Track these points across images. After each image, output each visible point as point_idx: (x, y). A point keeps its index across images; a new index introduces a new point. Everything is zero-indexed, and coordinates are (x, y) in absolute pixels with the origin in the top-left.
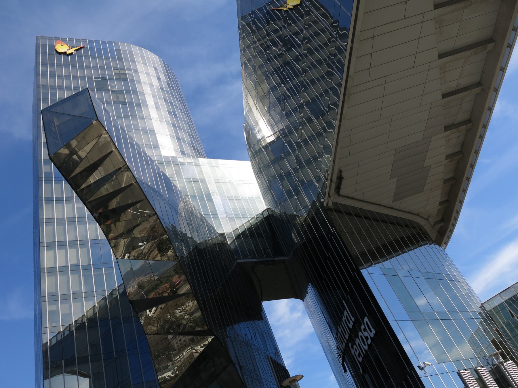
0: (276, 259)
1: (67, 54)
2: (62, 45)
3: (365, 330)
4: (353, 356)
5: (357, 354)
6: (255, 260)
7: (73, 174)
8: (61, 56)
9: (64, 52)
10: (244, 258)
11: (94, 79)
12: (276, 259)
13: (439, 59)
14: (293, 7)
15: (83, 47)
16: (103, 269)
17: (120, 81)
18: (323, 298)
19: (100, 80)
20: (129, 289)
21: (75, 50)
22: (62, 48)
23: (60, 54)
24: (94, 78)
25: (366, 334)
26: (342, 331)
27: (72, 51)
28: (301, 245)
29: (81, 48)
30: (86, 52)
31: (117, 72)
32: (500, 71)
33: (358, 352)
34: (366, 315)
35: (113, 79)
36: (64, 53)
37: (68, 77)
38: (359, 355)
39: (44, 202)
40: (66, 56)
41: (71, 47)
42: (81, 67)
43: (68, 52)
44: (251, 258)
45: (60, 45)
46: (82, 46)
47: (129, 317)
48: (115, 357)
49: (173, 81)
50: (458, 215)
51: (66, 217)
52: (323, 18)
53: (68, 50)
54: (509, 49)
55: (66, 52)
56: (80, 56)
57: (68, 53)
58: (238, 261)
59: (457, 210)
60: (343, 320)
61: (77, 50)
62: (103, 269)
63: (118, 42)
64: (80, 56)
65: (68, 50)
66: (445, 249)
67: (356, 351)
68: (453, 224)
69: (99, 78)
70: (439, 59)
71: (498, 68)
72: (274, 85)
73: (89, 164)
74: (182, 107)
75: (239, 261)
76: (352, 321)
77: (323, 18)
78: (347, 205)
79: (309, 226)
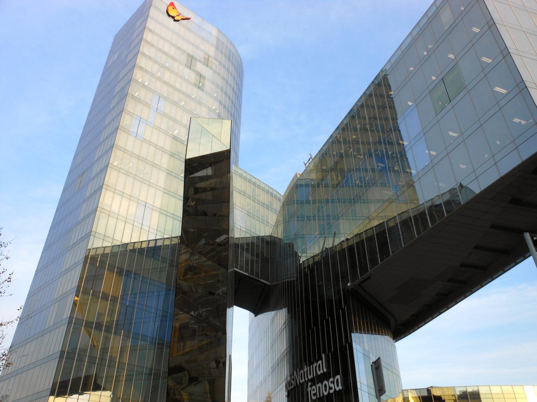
0: (262, 280)
2: (174, 9)
3: (333, 382)
4: (307, 392)
5: (313, 392)
6: (247, 274)
7: (192, 176)
11: (363, 184)
13: (490, 228)
16: (97, 266)
21: (182, 19)
23: (169, 16)
25: (332, 385)
26: (307, 371)
33: (315, 392)
34: (339, 374)
38: (314, 395)
48: (127, 305)
53: (177, 16)
57: (176, 19)
60: (314, 365)
62: (97, 266)
65: (177, 16)
66: (395, 342)
67: (314, 390)
70: (490, 228)
73: (203, 171)
75: (236, 269)
76: (322, 371)
78: (233, 195)
79: (306, 274)
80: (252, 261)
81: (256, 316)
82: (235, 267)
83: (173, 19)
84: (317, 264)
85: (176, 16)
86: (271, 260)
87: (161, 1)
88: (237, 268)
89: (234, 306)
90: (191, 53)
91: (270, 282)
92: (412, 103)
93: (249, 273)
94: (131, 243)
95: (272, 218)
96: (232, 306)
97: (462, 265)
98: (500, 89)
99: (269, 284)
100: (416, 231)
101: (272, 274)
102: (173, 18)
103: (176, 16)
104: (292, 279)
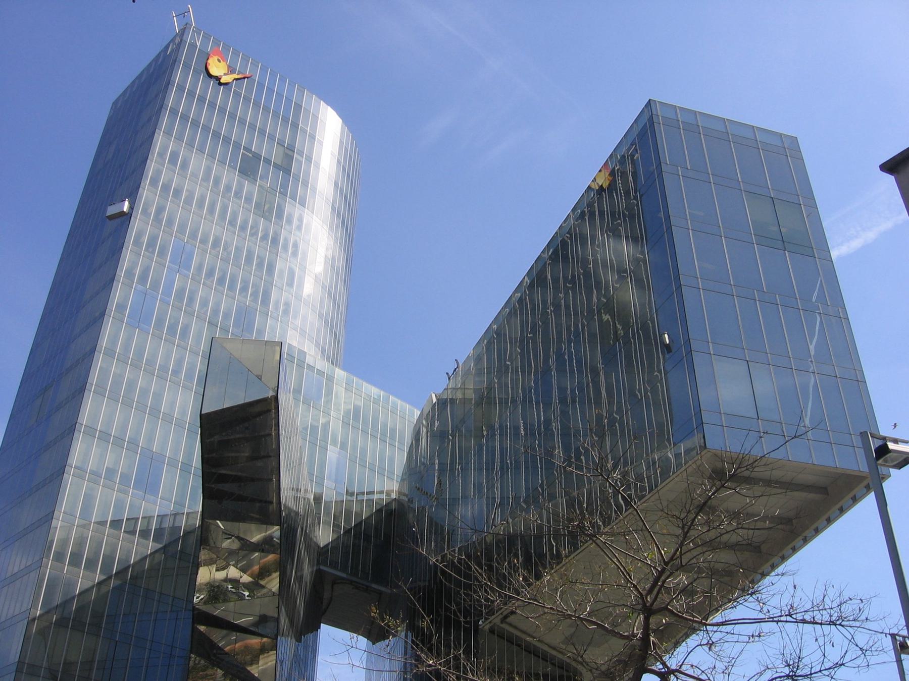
1: (220, 82)
2: (219, 61)
6: (344, 575)
9: (217, 76)
10: (331, 566)
12: (374, 586)
15: (247, 78)
17: (279, 171)
18: (510, 470)
19: (251, 155)
22: (217, 68)
23: (210, 76)
24: (243, 149)
29: (244, 78)
32: (837, 510)
36: (218, 79)
41: (231, 70)
44: (340, 571)
45: (216, 58)
49: (349, 236)
50: (839, 515)
52: (496, 492)
53: (225, 74)
54: (865, 490)
55: (220, 79)
57: (222, 81)
59: (843, 507)
61: (237, 79)
63: (201, 31)
65: (225, 74)
68: (855, 496)
71: (791, 546)
77: (496, 492)
81: (373, 644)
83: (218, 81)
102: (216, 80)
103: (223, 74)
104: (422, 584)
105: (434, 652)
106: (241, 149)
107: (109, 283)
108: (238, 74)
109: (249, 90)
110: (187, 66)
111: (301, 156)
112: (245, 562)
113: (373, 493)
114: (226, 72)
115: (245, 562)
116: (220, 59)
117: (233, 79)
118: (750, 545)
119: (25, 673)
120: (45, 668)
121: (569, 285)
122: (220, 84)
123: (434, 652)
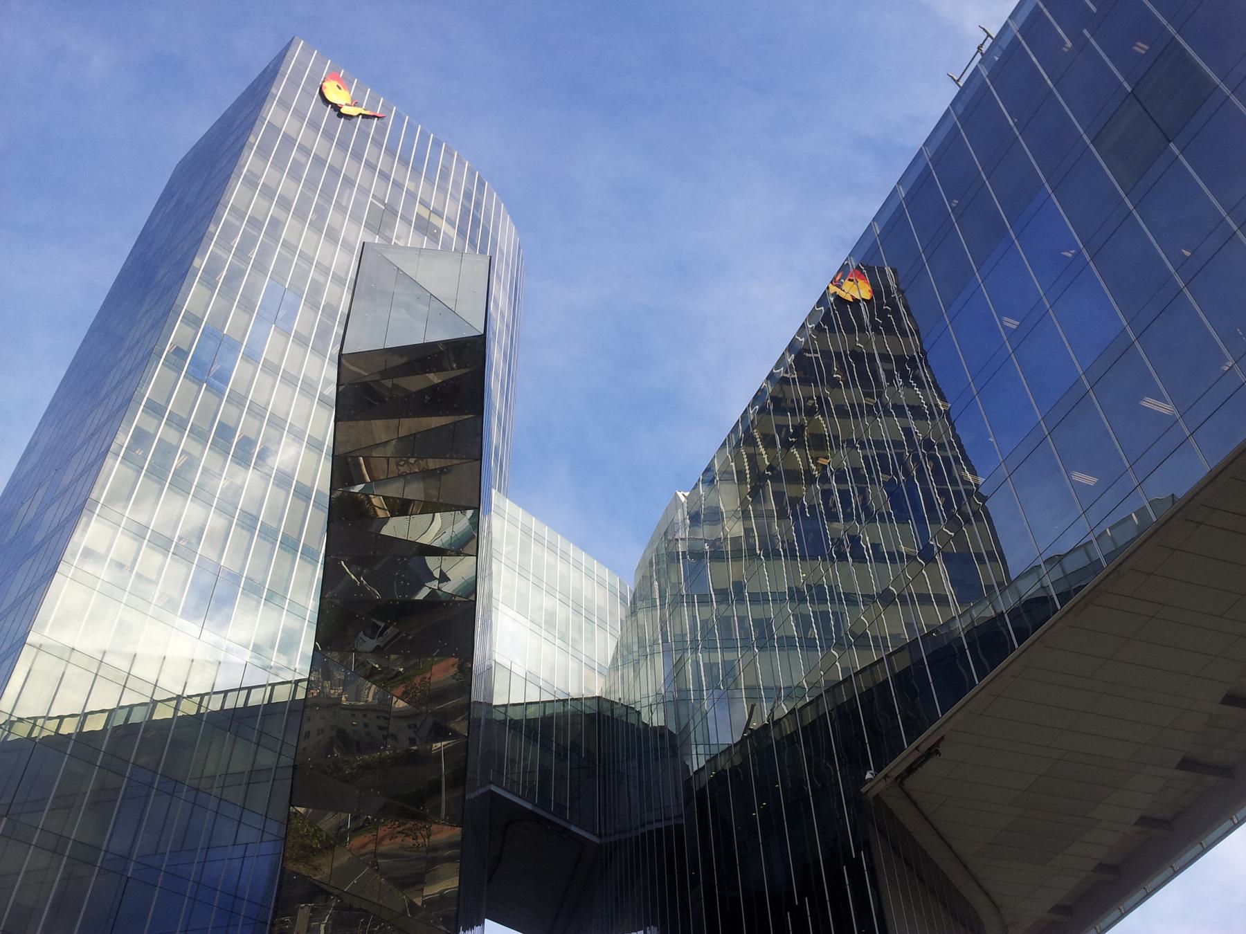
0: (574, 829)
1: (340, 112)
6: (529, 806)
8: (325, 107)
9: (336, 104)
14: (851, 300)
20: (266, 759)
21: (360, 114)
22: (336, 94)
27: (353, 111)
28: (645, 833)
29: (374, 116)
30: (381, 131)
31: (425, 213)
35: (374, 168)
36: (336, 108)
37: (319, 161)
39: (142, 407)
40: (336, 117)
42: (357, 156)
43: (344, 110)
46: (378, 113)
47: (221, 799)
48: (129, 875)
51: (245, 575)
53: (346, 105)
55: (341, 108)
56: (363, 135)
57: (343, 110)
58: (492, 789)
61: (365, 116)
64: (363, 135)
65: (346, 105)
69: (382, 202)
72: (804, 562)
74: (507, 340)
75: (494, 788)
80: (545, 772)
82: (491, 783)
83: (337, 113)
84: (739, 773)
85: (344, 104)
86: (601, 768)
87: (1243, 451)
88: (500, 786)
89: (486, 920)
90: (308, 920)
91: (600, 836)
92: (1095, 480)
93: (535, 805)
94: (123, 707)
95: (604, 646)
96: (481, 923)
97: (1143, 820)
98: (1156, 408)
99: (597, 840)
100: (416, 136)
101: (605, 792)
102: (335, 110)
103: (344, 104)
105: (667, 736)
106: (369, 197)
107: (162, 318)
108: (365, 110)
109: (381, 131)
110: (294, 83)
111: (464, 236)
112: (845, 867)
113: (670, 818)
114: (350, 103)
115: (845, 867)
116: (340, 86)
117: (358, 113)
118: (402, 848)
119: (35, 846)
120: (74, 840)
121: (838, 376)
122: (341, 115)
123: (667, 736)
